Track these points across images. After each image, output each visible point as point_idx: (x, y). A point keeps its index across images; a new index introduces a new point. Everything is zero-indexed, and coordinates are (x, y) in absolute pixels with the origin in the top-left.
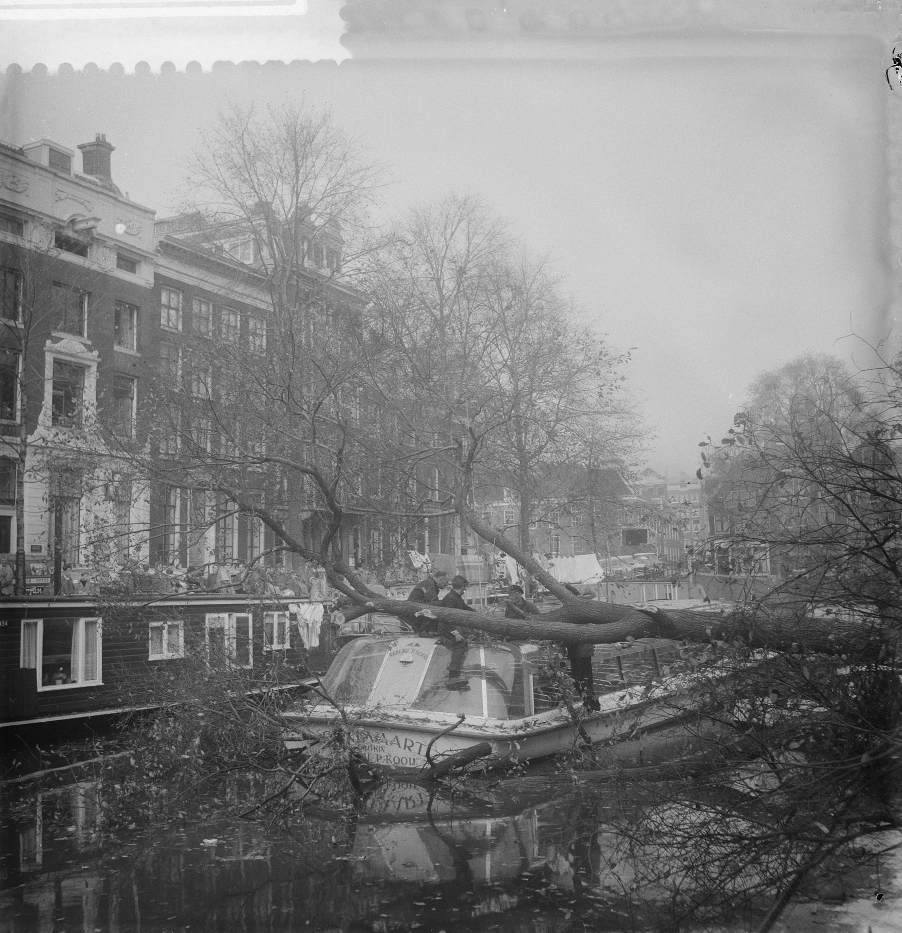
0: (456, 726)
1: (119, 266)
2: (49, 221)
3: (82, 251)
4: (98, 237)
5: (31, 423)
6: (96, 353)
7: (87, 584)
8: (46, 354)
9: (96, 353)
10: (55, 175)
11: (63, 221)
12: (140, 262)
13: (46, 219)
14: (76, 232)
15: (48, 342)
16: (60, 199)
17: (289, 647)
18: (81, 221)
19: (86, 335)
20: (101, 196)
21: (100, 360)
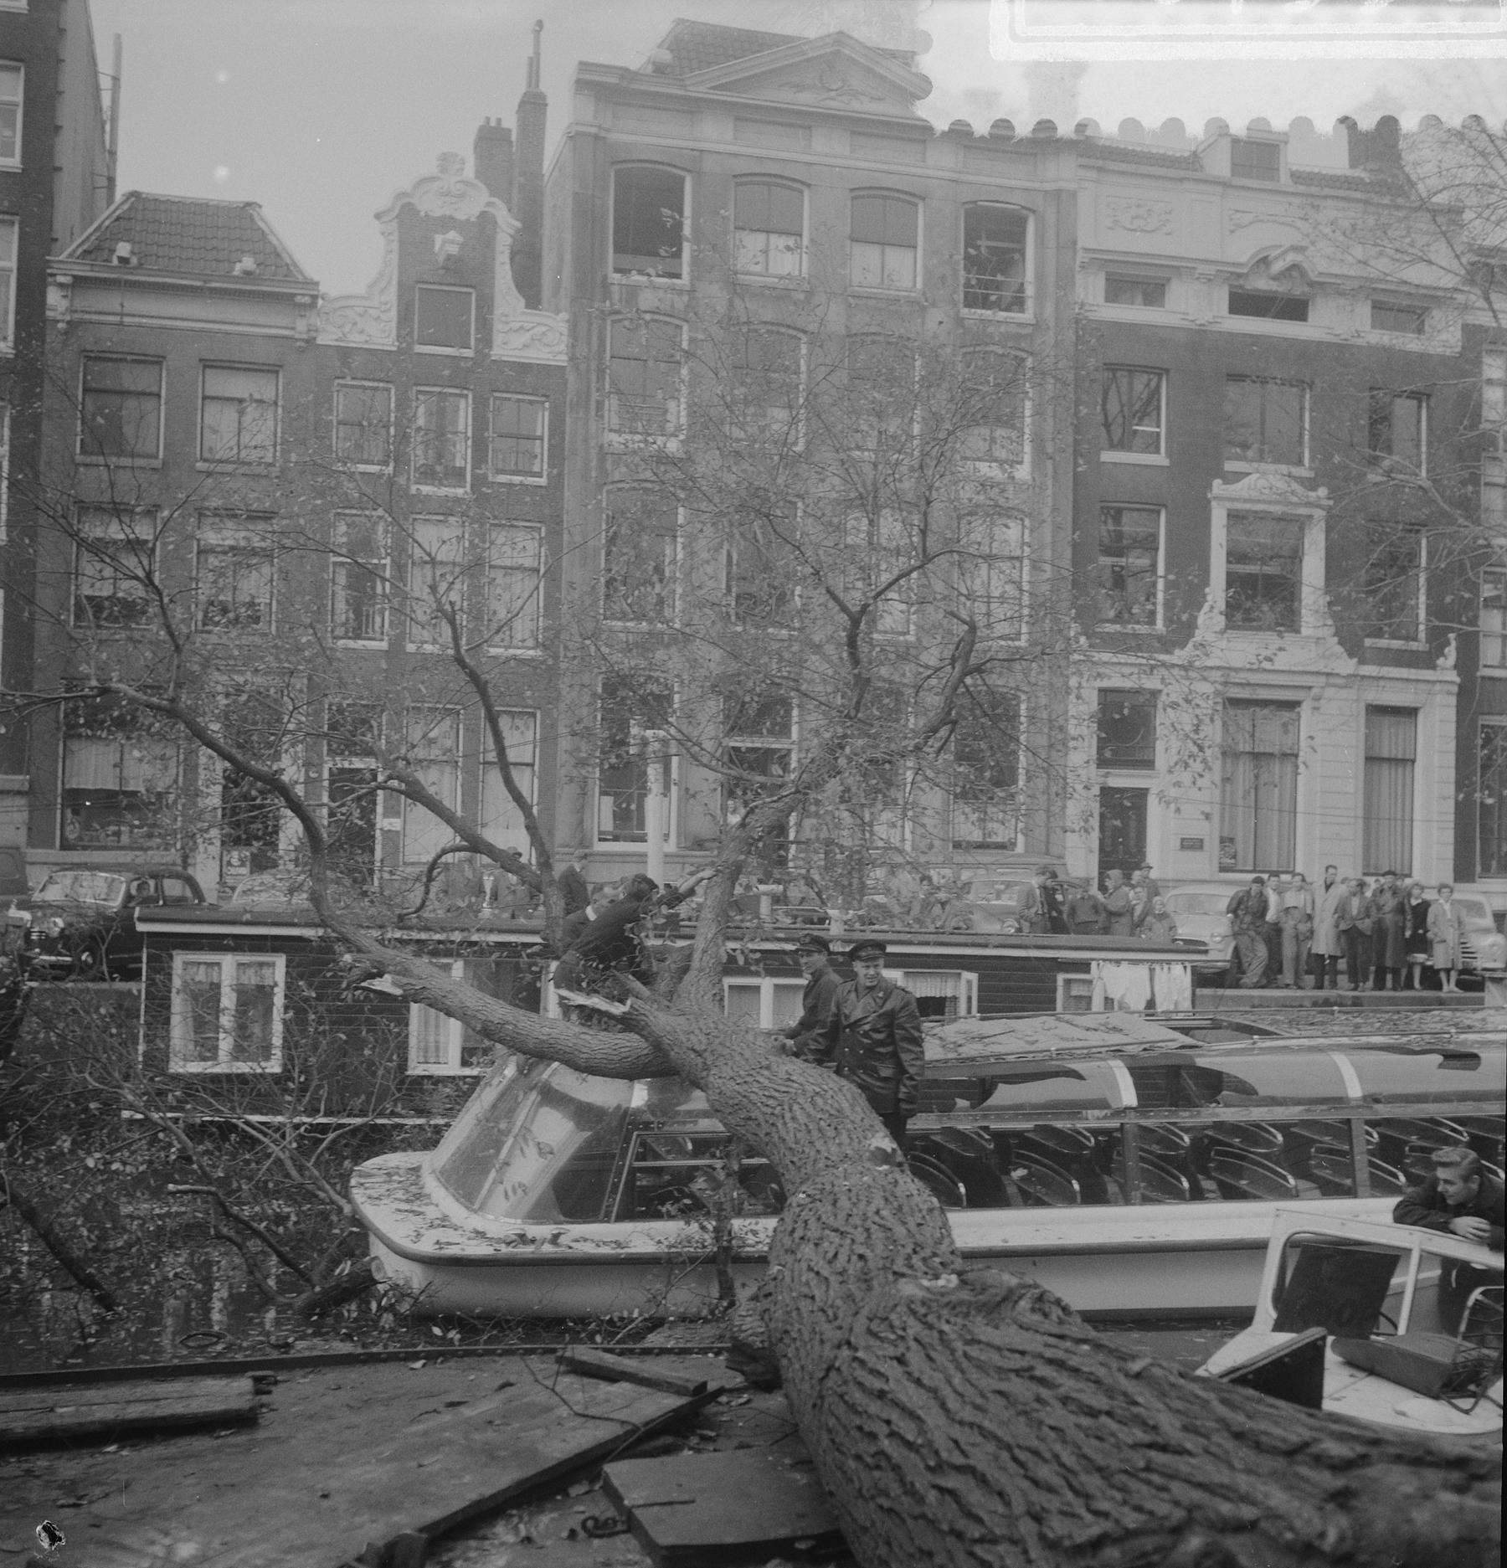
0: (1218, 1430)
1: (1234, 309)
2: (1211, 270)
3: (1296, 309)
4: (1321, 279)
5: (1182, 631)
6: (1322, 492)
7: (948, 907)
8: (1214, 504)
9: (1322, 492)
10: (1100, 169)
11: (1240, 265)
12: (1169, 280)
13: (1201, 268)
14: (1274, 278)
15: (1217, 483)
16: (1241, 227)
17: (277, 1069)
18: (1276, 258)
19: (1163, 450)
20: (1186, 185)
21: (1331, 503)
